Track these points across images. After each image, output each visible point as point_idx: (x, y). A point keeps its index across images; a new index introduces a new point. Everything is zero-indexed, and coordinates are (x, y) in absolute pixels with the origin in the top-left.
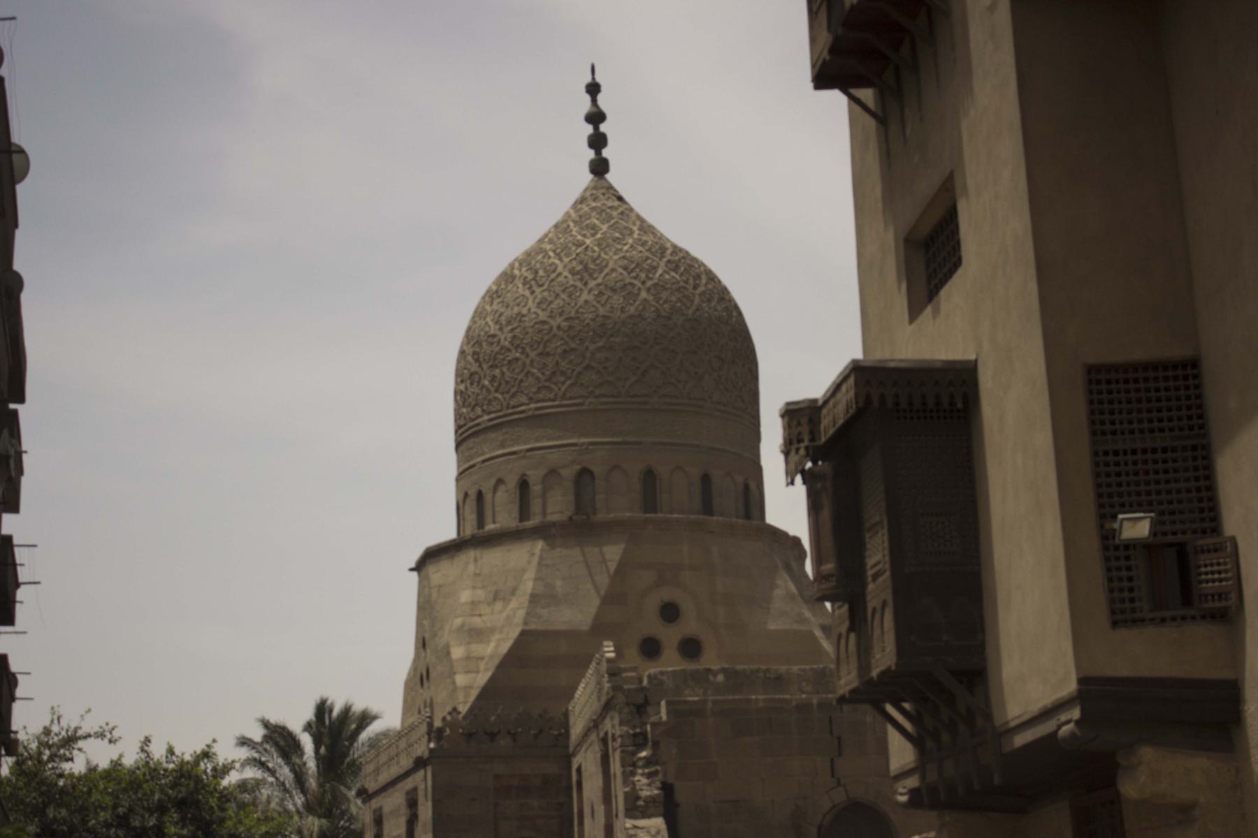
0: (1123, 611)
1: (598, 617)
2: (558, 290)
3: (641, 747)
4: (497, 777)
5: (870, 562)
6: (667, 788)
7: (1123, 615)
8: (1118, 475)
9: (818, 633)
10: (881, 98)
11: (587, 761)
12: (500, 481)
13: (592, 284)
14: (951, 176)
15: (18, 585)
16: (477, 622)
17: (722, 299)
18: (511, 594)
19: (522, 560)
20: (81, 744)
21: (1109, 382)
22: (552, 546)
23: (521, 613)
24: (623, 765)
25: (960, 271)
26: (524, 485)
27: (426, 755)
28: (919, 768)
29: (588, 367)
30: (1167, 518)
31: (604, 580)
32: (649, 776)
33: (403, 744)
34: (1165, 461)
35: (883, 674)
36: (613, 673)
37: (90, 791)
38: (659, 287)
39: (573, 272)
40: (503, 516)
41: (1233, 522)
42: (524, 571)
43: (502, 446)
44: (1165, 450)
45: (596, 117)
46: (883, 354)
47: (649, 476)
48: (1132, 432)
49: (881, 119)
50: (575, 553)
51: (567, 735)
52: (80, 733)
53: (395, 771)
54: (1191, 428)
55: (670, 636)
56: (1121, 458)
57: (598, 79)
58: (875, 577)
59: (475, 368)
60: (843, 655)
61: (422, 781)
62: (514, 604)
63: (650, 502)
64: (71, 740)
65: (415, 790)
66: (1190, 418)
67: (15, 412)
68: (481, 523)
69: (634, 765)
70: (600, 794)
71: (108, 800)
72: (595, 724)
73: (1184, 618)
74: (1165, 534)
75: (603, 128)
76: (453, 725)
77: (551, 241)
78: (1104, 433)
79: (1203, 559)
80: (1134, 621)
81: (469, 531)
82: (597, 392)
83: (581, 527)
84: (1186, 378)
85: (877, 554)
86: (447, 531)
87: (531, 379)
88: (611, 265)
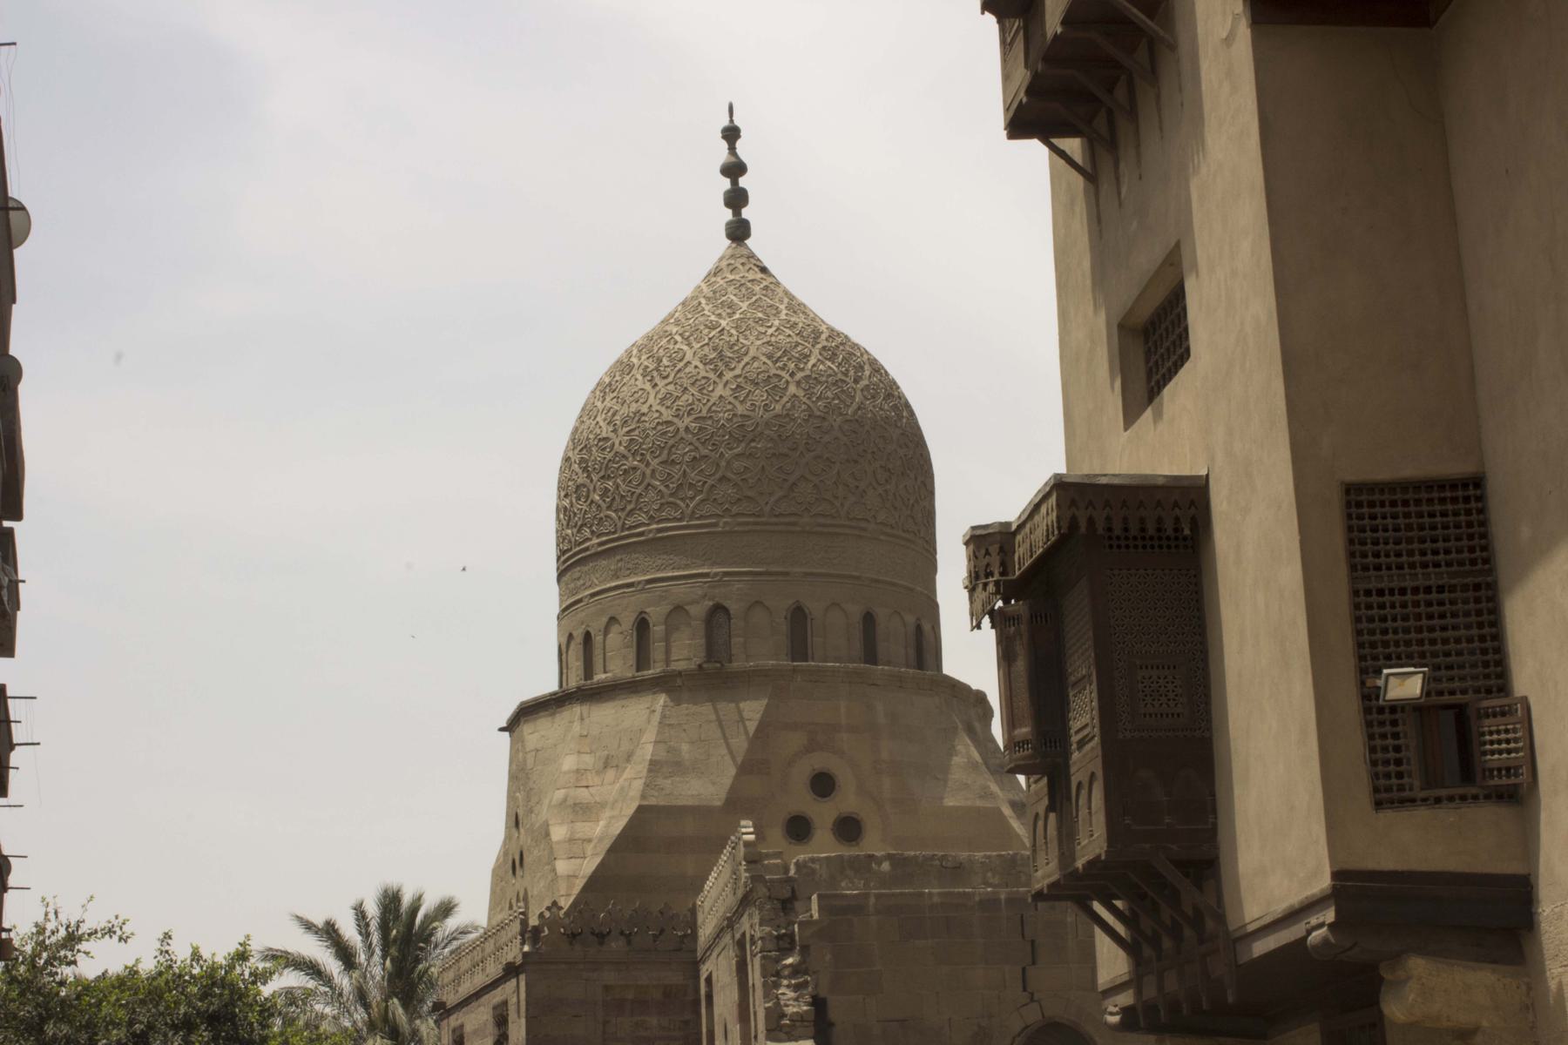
0: (1388, 789)
2: (686, 382)
3: (788, 951)
4: (607, 988)
5: (1075, 725)
6: (818, 1003)
8: (1384, 619)
9: (1007, 811)
11: (719, 968)
12: (613, 620)
13: (728, 375)
15: (12, 747)
16: (583, 795)
17: (889, 396)
18: (622, 764)
19: (639, 718)
20: (84, 946)
21: (1372, 504)
22: (678, 702)
23: (638, 785)
25: (1187, 365)
26: (642, 625)
27: (519, 960)
29: (723, 479)
31: (740, 744)
32: (796, 988)
33: (490, 946)
35: (1090, 864)
36: (753, 860)
37: (99, 1004)
38: (812, 380)
39: (705, 361)
40: (617, 664)
41: (1524, 681)
44: (1441, 589)
45: (734, 169)
47: (798, 615)
49: (1091, 176)
50: (706, 709)
51: (694, 936)
52: (84, 929)
53: (480, 980)
54: (1473, 562)
56: (1387, 598)
57: (737, 122)
58: (1081, 744)
61: (514, 993)
62: (627, 774)
63: (799, 647)
64: (72, 939)
65: (505, 1003)
68: (588, 672)
70: (735, 1011)
71: (122, 1014)
72: (730, 923)
73: (1463, 798)
74: (1441, 693)
75: (743, 182)
76: (553, 923)
77: (677, 323)
78: (1365, 568)
80: (1402, 801)
81: (574, 682)
82: (735, 510)
83: (712, 678)
84: (1467, 499)
85: (1084, 715)
86: (547, 683)
87: (652, 494)
88: (752, 353)
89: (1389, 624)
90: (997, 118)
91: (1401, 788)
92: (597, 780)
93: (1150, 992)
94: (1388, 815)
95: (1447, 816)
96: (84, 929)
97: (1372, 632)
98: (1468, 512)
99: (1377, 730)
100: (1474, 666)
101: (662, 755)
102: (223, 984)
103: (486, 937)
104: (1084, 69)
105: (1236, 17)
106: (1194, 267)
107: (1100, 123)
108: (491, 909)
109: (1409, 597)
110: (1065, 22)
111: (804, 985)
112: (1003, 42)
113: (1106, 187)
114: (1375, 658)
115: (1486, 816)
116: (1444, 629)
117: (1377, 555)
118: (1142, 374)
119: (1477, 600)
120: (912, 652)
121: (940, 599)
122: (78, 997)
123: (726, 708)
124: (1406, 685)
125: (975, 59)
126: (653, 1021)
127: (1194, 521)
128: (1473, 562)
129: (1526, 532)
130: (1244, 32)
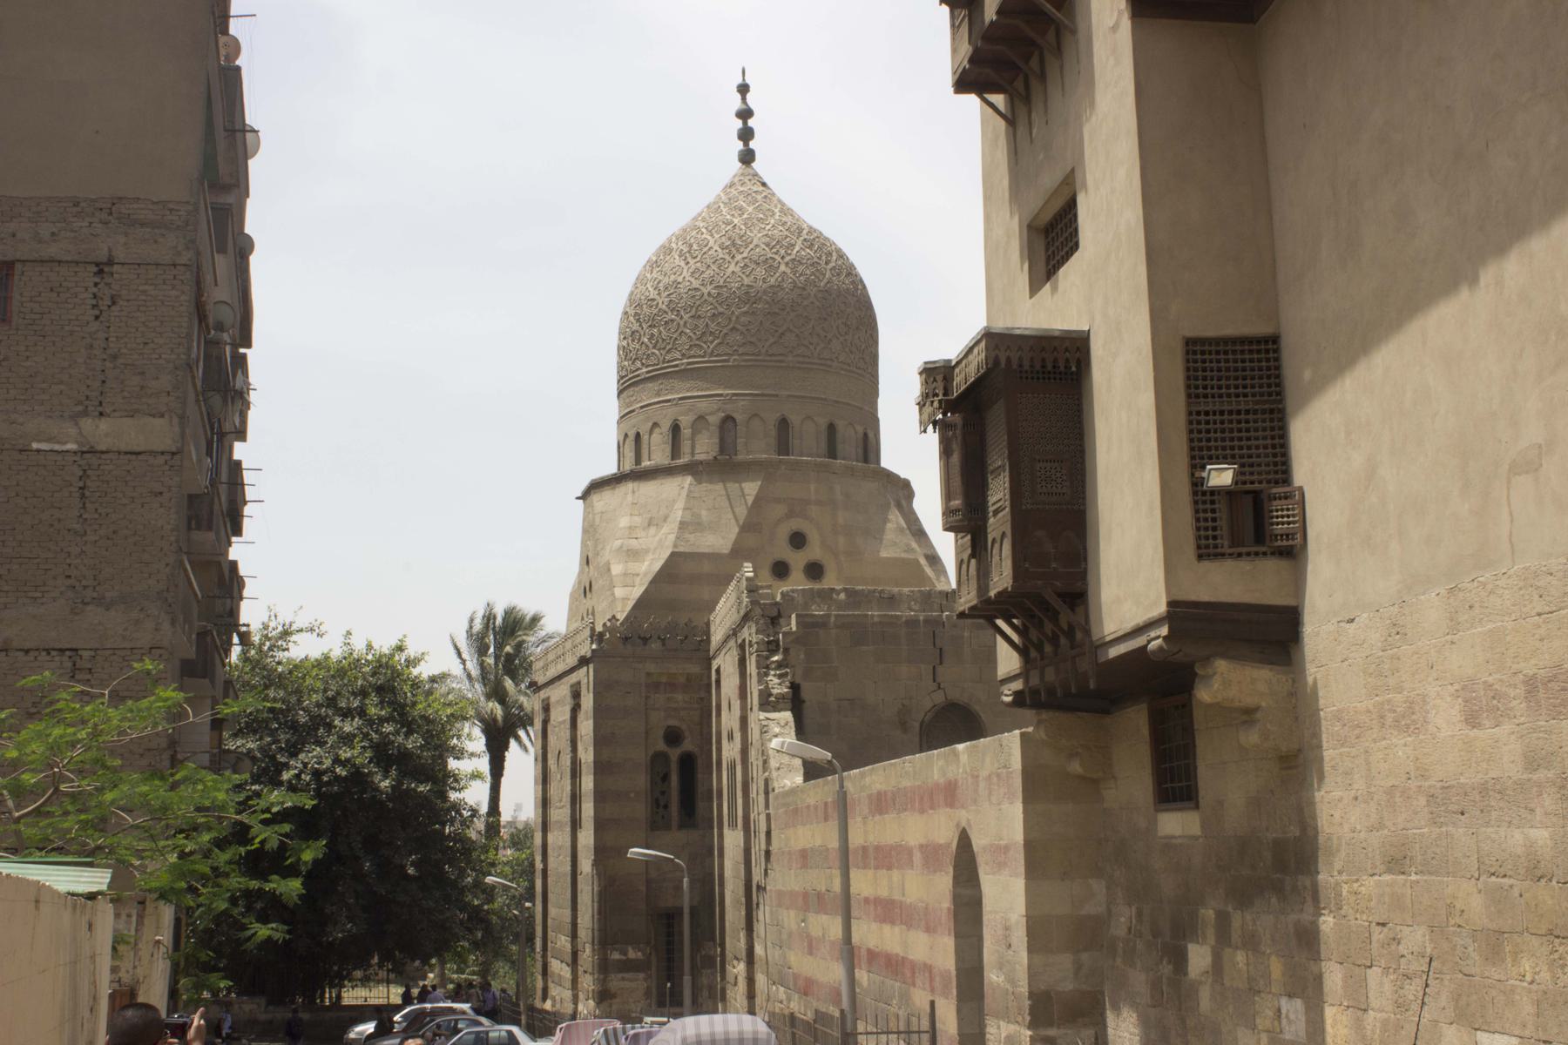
0: (1207, 547)
1: (736, 542)
2: (709, 261)
3: (774, 652)
5: (992, 500)
6: (795, 687)
7: (1207, 550)
8: (1208, 431)
9: (923, 561)
10: (1011, 103)
11: (726, 663)
12: (655, 425)
13: (739, 257)
14: (1073, 170)
15: (245, 503)
17: (849, 274)
18: (664, 522)
19: (673, 492)
20: (294, 638)
21: (1203, 353)
23: (672, 537)
24: (758, 667)
25: (1076, 255)
26: (676, 429)
27: (589, 654)
28: (1024, 674)
29: (733, 329)
30: (1247, 469)
31: (742, 512)
32: (780, 676)
33: (568, 645)
34: (1247, 422)
35: (1000, 594)
36: (752, 590)
37: (303, 678)
38: (796, 262)
39: (722, 247)
40: (658, 455)
41: (1301, 474)
42: (674, 501)
43: (658, 395)
44: (1247, 412)
45: (745, 114)
46: (1000, 325)
47: (784, 424)
48: (1221, 396)
49: (1011, 121)
50: (719, 487)
51: (708, 641)
52: (294, 627)
54: (1270, 394)
55: (798, 560)
56: (1211, 417)
58: (996, 512)
59: (636, 327)
60: (964, 577)
61: (585, 676)
62: (665, 530)
63: (783, 446)
64: (286, 633)
65: (579, 683)
66: (1269, 386)
67: (245, 355)
68: (638, 460)
69: (767, 667)
70: (737, 691)
71: (319, 684)
72: (734, 632)
73: (1257, 554)
74: (1244, 483)
75: (751, 123)
76: (612, 630)
77: (704, 220)
78: (1197, 396)
79: (1276, 504)
80: (1216, 555)
81: (628, 466)
82: (741, 350)
83: (723, 466)
84: (1267, 351)
85: (999, 492)
86: (610, 468)
89: (1212, 435)
90: (947, 79)
91: (1216, 547)
92: (643, 534)
93: (1035, 681)
94: (1206, 564)
95: (1244, 565)
96: (294, 627)
97: (1200, 440)
98: (1268, 360)
99: (1201, 506)
100: (1268, 465)
101: (688, 518)
102: (387, 666)
103: (566, 638)
104: (1012, 42)
105: (1120, 13)
106: (1084, 185)
107: (1019, 84)
108: (569, 620)
109: (1226, 417)
110: (998, 13)
111: (786, 674)
112: (953, 26)
113: (1022, 129)
114: (1202, 458)
115: (1271, 565)
116: (1248, 439)
117: (1205, 387)
118: (1043, 258)
119: (1272, 420)
120: (860, 451)
121: (880, 415)
122: (291, 672)
123: (733, 487)
124: (1221, 476)
125: (935, 42)
126: (679, 697)
127: (1079, 362)
128: (1270, 394)
129: (1307, 374)
130: (1126, 24)
